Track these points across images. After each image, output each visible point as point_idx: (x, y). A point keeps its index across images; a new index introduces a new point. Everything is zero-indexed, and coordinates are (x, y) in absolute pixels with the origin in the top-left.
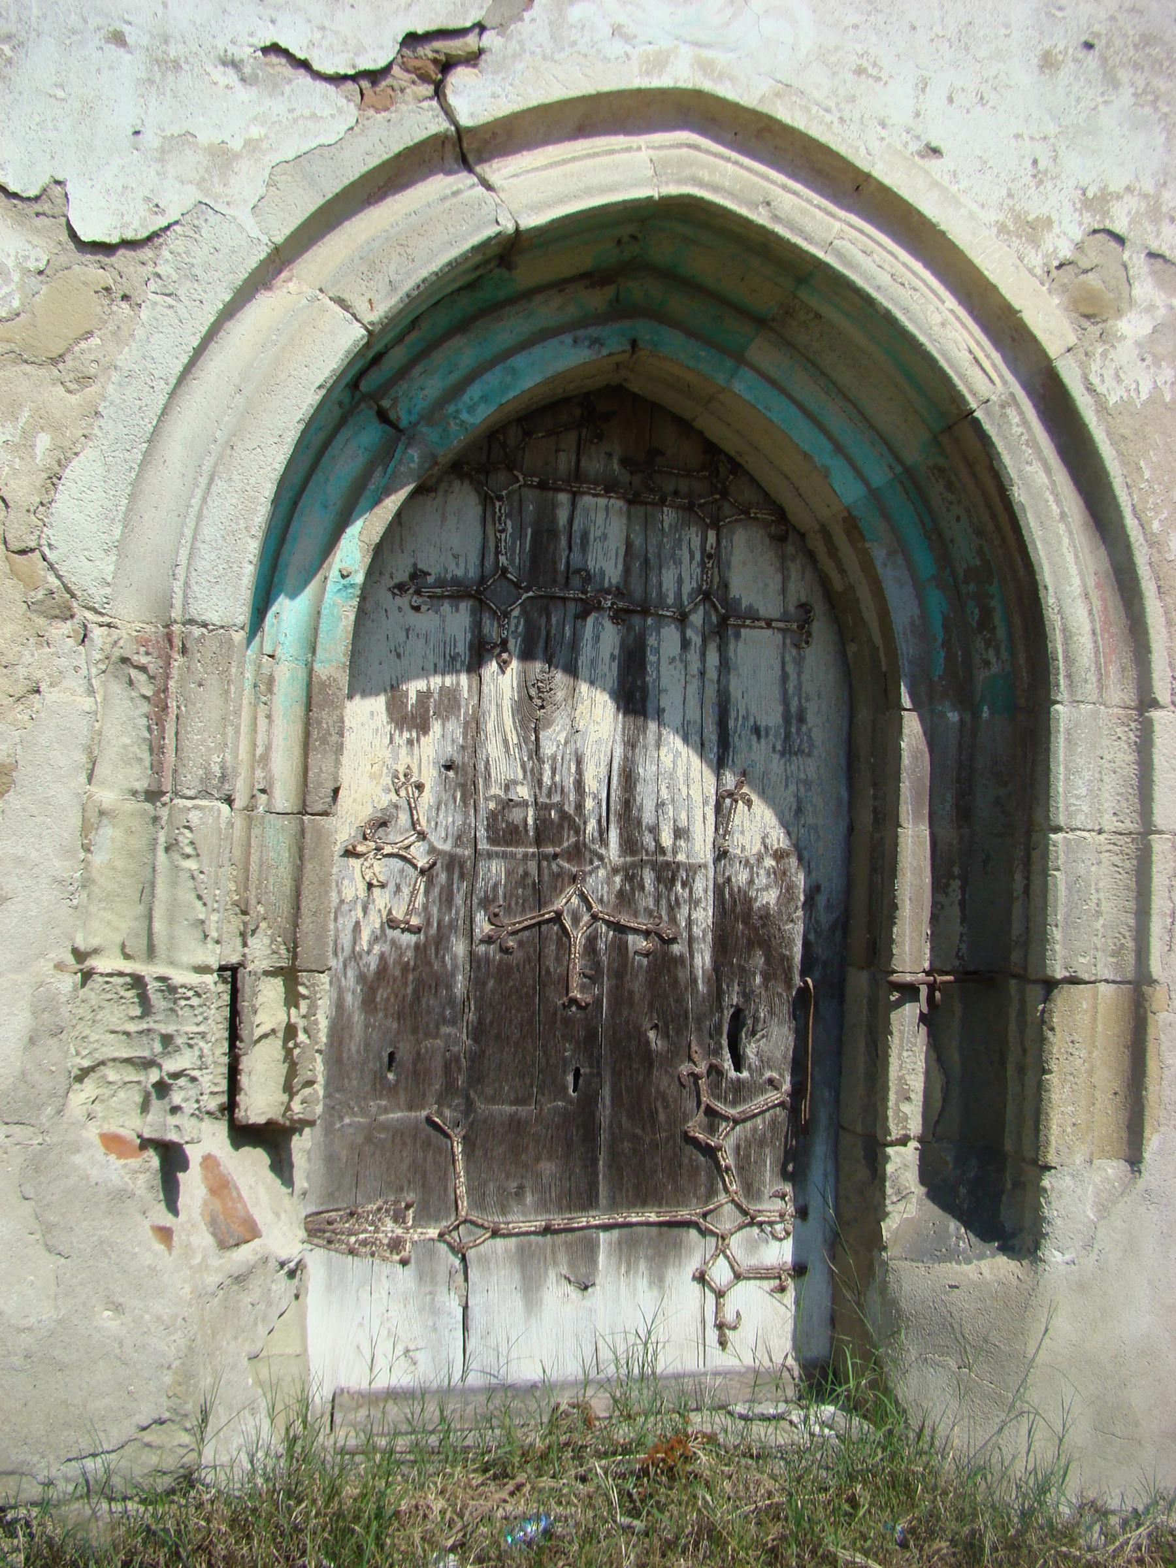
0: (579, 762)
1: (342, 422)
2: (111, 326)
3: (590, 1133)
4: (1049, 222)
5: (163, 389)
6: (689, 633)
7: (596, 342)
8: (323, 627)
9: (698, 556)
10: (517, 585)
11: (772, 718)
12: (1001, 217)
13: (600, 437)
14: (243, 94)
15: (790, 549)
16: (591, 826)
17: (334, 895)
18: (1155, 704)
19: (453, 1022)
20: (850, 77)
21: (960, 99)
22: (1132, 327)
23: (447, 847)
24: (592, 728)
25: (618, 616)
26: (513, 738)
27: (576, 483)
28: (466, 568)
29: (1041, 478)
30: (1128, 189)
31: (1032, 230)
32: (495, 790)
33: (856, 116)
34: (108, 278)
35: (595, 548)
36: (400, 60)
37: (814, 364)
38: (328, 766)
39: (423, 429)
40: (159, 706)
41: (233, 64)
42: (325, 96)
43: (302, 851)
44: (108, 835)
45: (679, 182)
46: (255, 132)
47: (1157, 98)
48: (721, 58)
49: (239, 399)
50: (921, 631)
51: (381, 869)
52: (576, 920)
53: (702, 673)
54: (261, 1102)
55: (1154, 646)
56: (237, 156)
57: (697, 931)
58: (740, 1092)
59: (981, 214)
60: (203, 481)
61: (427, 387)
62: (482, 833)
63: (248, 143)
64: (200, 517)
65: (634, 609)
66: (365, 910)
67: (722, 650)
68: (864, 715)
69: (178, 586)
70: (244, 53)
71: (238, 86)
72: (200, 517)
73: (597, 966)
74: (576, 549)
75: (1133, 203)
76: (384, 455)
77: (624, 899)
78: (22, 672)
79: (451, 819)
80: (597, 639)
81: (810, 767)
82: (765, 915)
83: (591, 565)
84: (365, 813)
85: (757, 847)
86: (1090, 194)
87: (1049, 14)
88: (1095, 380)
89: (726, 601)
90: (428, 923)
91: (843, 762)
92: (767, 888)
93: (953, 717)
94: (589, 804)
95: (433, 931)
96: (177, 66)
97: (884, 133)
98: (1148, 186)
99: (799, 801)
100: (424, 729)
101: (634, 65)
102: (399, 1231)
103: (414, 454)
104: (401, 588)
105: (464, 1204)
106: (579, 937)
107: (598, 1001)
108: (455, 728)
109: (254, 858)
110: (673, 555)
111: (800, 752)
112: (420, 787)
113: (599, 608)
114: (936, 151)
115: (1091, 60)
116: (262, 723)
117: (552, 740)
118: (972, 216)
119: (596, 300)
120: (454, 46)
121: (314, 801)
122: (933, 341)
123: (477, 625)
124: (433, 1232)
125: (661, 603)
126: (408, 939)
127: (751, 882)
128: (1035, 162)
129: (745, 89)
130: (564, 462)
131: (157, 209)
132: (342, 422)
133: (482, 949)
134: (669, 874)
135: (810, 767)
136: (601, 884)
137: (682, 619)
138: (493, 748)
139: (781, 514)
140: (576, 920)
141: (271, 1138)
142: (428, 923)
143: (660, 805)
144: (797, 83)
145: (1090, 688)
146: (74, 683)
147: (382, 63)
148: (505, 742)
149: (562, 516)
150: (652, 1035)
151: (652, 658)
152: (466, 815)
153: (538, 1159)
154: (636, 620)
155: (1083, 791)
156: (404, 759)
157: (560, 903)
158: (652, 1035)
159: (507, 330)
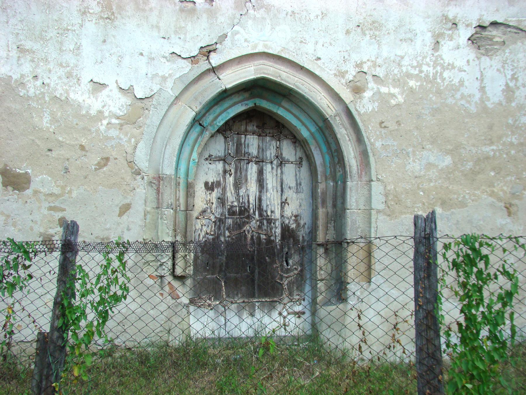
0: (248, 197)
1: (192, 127)
2: (144, 115)
3: (253, 281)
4: (347, 71)
5: (156, 128)
6: (273, 166)
7: (247, 104)
8: (190, 171)
9: (275, 148)
10: (233, 157)
11: (293, 184)
12: (335, 72)
13: (251, 121)
14: (167, 64)
15: (297, 145)
16: (252, 211)
17: (194, 227)
18: (372, 181)
19: (221, 255)
20: (299, 44)
21: (325, 45)
22: (368, 94)
23: (219, 216)
24: (251, 189)
25: (257, 163)
26: (233, 192)
27: (246, 132)
28: (221, 154)
29: (344, 132)
30: (368, 60)
31: (342, 74)
32: (229, 203)
33: (300, 53)
34: (143, 105)
35: (251, 147)
36: (200, 53)
37: (297, 105)
38: (192, 200)
39: (209, 127)
40: (158, 191)
41: (166, 58)
42: (184, 63)
43: (187, 218)
44: (149, 217)
45: (260, 74)
46: (170, 72)
47: (376, 37)
48: (269, 43)
49: (171, 129)
50: (324, 164)
51: (204, 222)
52: (248, 232)
53: (277, 175)
54: (179, 271)
55: (372, 168)
56: (167, 78)
57: (277, 234)
58: (288, 271)
59: (330, 72)
60: (164, 146)
61: (209, 118)
62: (227, 213)
63: (169, 74)
64: (164, 153)
65: (260, 161)
66: (201, 231)
67: (281, 169)
68: (314, 184)
69: (161, 167)
70: (167, 55)
71: (167, 62)
72: (164, 153)
73: (254, 242)
74: (246, 148)
75: (369, 63)
76: (201, 133)
77: (260, 227)
78: (132, 186)
79: (220, 210)
80: (252, 168)
81: (302, 196)
82: (293, 230)
83: (250, 151)
84: (201, 209)
85: (290, 214)
86: (358, 63)
87: (348, 20)
88: (358, 108)
89: (282, 158)
90: (215, 233)
91: (311, 194)
92: (293, 224)
93: (332, 184)
94: (251, 206)
95: (216, 235)
96: (154, 59)
97: (307, 56)
98: (373, 59)
99: (300, 203)
100: (213, 190)
101: (250, 48)
102: (210, 302)
103: (208, 133)
104: (207, 159)
105: (225, 296)
106: (249, 236)
107: (254, 251)
108: (220, 190)
109: (177, 220)
110: (269, 148)
111: (300, 192)
112: (212, 203)
113: (252, 161)
114: (319, 59)
115: (359, 30)
116: (178, 192)
117: (242, 192)
118: (328, 72)
119: (246, 95)
120: (211, 48)
121: (189, 208)
122: (318, 103)
123: (224, 166)
124: (218, 303)
125: (266, 159)
126: (211, 237)
127: (289, 223)
128: (344, 57)
129: (274, 50)
130: (243, 128)
131: (152, 90)
132: (192, 127)
133: (227, 239)
134: (270, 221)
135: (302, 196)
136: (254, 224)
137: (271, 163)
138: (229, 194)
139: (295, 137)
140: (248, 232)
141: (181, 278)
142: (215, 233)
143: (267, 206)
144: (286, 47)
145: (356, 177)
146: (142, 187)
147: (196, 54)
148: (231, 193)
149: (243, 140)
150: (267, 258)
151: (264, 172)
152: (223, 209)
153: (241, 286)
154: (261, 163)
155: (354, 201)
156: (209, 197)
157: (245, 228)
158: (267, 258)
159: (226, 104)
